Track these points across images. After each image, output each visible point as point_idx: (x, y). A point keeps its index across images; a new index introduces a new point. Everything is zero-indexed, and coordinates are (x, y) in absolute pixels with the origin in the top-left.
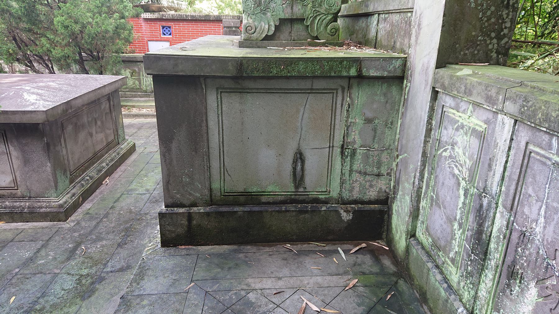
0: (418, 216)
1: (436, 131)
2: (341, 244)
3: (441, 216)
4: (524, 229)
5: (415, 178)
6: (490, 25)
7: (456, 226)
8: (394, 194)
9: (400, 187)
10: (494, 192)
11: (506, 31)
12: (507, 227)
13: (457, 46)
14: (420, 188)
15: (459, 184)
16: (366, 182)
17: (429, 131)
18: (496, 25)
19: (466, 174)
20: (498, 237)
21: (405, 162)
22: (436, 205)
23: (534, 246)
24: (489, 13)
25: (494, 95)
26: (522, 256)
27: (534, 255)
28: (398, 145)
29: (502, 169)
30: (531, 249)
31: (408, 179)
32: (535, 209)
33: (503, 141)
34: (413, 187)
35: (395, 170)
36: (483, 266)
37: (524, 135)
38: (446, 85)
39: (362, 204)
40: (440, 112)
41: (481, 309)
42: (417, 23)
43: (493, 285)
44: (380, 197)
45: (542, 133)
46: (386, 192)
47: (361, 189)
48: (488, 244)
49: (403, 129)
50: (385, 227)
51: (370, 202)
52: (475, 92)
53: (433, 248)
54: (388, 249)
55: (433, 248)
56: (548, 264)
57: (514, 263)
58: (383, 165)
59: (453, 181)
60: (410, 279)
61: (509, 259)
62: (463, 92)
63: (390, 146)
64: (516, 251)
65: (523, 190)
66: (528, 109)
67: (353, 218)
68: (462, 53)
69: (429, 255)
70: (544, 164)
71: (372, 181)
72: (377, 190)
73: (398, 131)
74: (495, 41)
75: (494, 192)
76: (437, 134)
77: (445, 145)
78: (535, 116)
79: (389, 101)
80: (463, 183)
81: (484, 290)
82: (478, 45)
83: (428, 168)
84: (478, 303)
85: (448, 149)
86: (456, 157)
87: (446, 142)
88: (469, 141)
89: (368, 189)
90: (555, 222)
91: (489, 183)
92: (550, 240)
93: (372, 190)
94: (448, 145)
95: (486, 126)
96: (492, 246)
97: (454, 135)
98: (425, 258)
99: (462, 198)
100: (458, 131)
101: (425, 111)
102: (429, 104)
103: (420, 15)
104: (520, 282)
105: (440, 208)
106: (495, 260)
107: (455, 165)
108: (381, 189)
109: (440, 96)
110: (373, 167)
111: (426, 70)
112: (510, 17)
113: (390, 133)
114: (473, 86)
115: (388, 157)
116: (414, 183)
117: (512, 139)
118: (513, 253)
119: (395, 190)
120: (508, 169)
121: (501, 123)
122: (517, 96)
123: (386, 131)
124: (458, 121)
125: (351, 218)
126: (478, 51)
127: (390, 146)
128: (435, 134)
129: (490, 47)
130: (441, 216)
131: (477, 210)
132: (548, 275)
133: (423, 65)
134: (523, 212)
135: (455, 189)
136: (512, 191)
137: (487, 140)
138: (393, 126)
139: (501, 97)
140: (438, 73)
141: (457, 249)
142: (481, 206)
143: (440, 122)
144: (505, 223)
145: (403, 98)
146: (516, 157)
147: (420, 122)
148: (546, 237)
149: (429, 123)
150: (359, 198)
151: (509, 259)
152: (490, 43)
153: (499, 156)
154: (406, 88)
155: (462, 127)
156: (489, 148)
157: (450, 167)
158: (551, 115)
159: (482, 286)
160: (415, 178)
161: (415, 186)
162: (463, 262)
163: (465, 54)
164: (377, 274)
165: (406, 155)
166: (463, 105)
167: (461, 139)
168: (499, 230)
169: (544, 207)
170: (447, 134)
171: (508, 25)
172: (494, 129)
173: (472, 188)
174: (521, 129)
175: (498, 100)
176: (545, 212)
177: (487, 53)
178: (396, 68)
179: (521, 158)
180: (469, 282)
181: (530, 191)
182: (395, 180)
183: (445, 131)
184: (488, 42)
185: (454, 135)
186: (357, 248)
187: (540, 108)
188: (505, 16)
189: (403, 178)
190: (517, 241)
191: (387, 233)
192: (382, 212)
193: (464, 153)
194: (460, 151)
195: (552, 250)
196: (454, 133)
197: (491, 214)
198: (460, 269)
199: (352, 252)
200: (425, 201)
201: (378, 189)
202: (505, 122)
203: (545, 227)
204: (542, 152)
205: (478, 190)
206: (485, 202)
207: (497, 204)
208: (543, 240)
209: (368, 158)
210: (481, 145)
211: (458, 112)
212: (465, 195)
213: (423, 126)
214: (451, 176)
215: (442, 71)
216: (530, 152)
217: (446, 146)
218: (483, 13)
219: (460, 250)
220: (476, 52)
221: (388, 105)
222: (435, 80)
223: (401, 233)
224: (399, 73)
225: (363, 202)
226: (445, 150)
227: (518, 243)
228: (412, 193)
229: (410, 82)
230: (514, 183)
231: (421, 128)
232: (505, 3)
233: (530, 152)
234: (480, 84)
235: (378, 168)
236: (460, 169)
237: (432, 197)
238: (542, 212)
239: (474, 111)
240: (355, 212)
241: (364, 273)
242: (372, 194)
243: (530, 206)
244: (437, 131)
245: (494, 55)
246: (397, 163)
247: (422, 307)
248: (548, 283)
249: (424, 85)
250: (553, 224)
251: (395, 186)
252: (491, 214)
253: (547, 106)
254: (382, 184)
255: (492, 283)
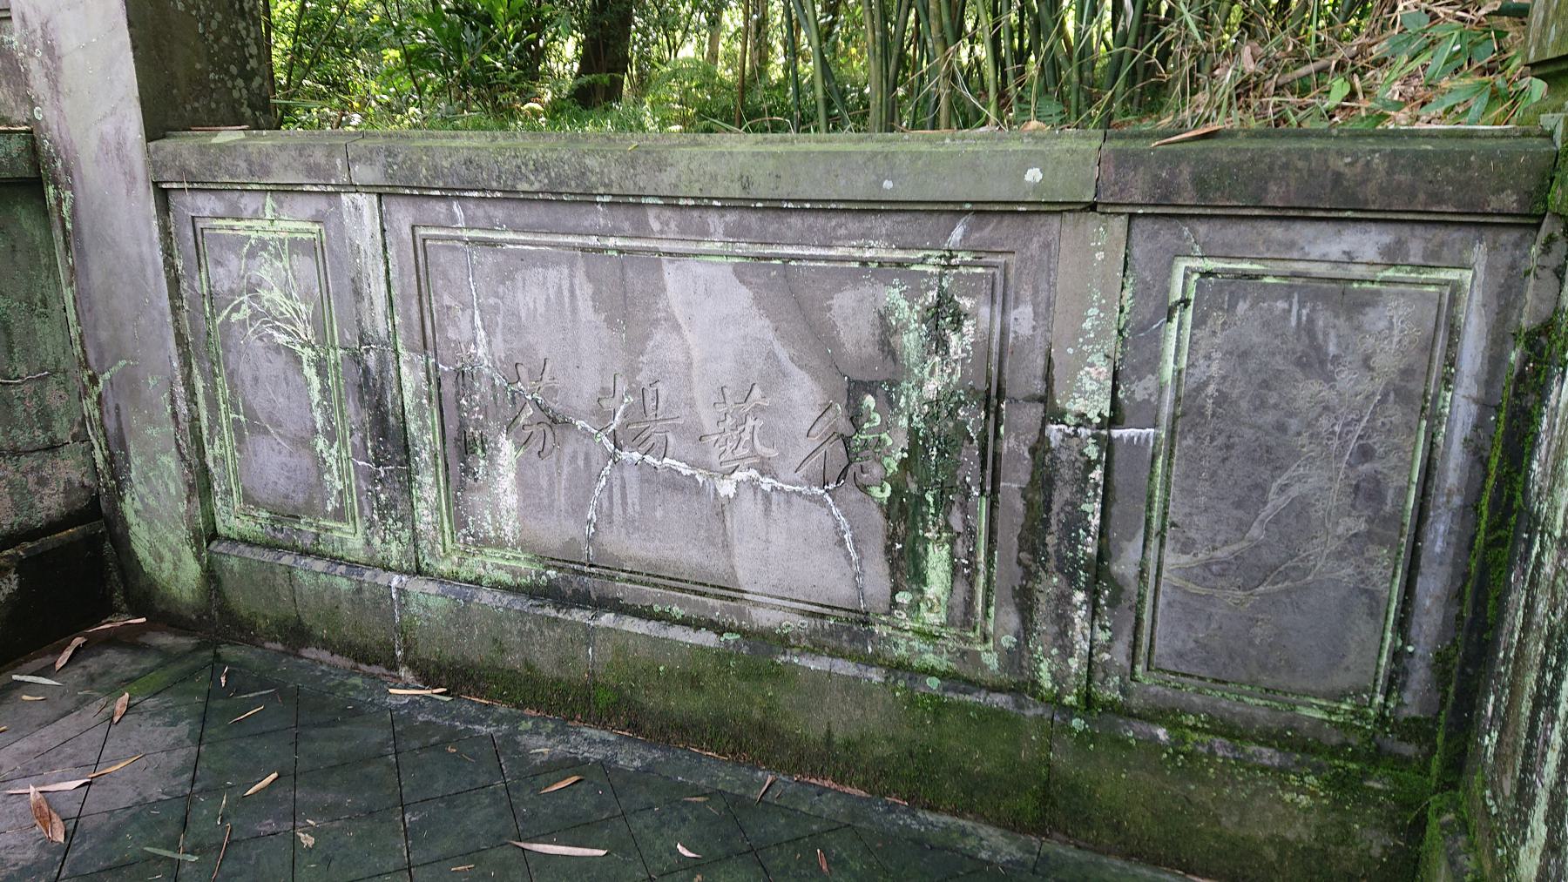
0: (209, 486)
1: (193, 278)
2: (15, 667)
3: (277, 448)
4: (459, 365)
5: (173, 401)
6: (222, 49)
7: (321, 443)
8: (113, 477)
9: (132, 447)
10: (383, 334)
11: (253, 63)
12: (429, 379)
13: (175, 91)
14: (195, 419)
15: (298, 360)
16: (25, 474)
17: (174, 282)
18: (233, 50)
19: (306, 331)
20: (420, 405)
21: (130, 383)
22: (251, 433)
23: (484, 380)
24: (214, 25)
25: (323, 161)
26: (472, 407)
27: (490, 392)
28: (84, 352)
29: (383, 287)
30: (482, 387)
31: (150, 415)
32: (464, 324)
33: (368, 239)
34: (177, 424)
35: (97, 416)
36: (409, 472)
37: (403, 216)
38: (193, 170)
39: (31, 540)
40: (191, 234)
41: (433, 548)
42: (39, 43)
43: (439, 491)
44: (73, 504)
45: (433, 203)
46: (83, 486)
47: (17, 497)
48: (405, 428)
49: (86, 307)
50: (115, 576)
51: (52, 527)
52: (275, 165)
53: (278, 526)
54: (144, 620)
55: (278, 526)
56: (513, 392)
57: (462, 427)
58: (56, 416)
59: (280, 362)
60: (242, 630)
61: (451, 428)
62: (246, 171)
63: (58, 362)
64: (459, 407)
65: (434, 306)
66: (401, 168)
67: (20, 584)
68: (188, 107)
69: (271, 546)
70: (454, 248)
71: (40, 467)
72: (61, 489)
73: (72, 317)
74: (240, 82)
75: (383, 334)
76: (197, 284)
77: (230, 297)
78: (415, 174)
79: (18, 247)
80: (307, 353)
81: (426, 512)
82: (213, 91)
83: (200, 368)
84: (422, 544)
85: (242, 302)
86: (268, 310)
87: (232, 291)
88: (291, 266)
89: (37, 492)
90: (500, 326)
91: (367, 323)
92: (503, 355)
93: (47, 491)
94: (240, 295)
95: (317, 227)
96: (413, 427)
97: (247, 269)
98: (268, 556)
99: (316, 383)
100: (254, 258)
101: (151, 239)
102: (155, 222)
103: (44, 25)
104: (484, 450)
105: (266, 432)
106: (428, 447)
107: (272, 328)
108: (69, 482)
109: (174, 200)
110: (32, 427)
111: (118, 150)
112: (253, 35)
113: (48, 330)
114: (267, 155)
115: (62, 392)
116: (175, 415)
117: (383, 230)
118: (455, 412)
119: (117, 466)
120: (394, 283)
121: (352, 210)
122: (371, 152)
123: (37, 326)
124: (249, 238)
125: (15, 585)
126: (217, 103)
127: (58, 362)
128: (192, 287)
129: (236, 94)
130: (277, 448)
131: (360, 386)
132: (519, 409)
133: (102, 139)
134: (448, 340)
135: (290, 374)
136: (416, 316)
137: (331, 250)
138: (49, 310)
139: (338, 161)
140: (157, 149)
141: (339, 485)
142: (366, 371)
143: (198, 254)
144: (422, 374)
145: (57, 233)
146: (401, 257)
147: (143, 270)
148: (496, 355)
149: (169, 265)
150: (20, 524)
151: (451, 428)
152: (234, 87)
153: (369, 267)
154: (59, 205)
155: (263, 245)
156: (340, 263)
157: (261, 339)
158: (442, 167)
159: (422, 509)
160: (173, 401)
161: (180, 420)
162: (363, 498)
163: (195, 110)
164: (160, 666)
165: (122, 363)
166: (248, 203)
167: (266, 270)
168: (417, 393)
169: (477, 312)
170: (223, 275)
171: (254, 50)
172: (341, 225)
173: (331, 350)
174: (393, 208)
175: (335, 167)
176: (482, 320)
177: (233, 107)
178: (12, 159)
179: (412, 255)
180: (391, 521)
181: (447, 300)
182: (107, 441)
183: (221, 270)
184: (229, 84)
185: (247, 269)
186: (68, 653)
187: (420, 160)
188: (244, 33)
189: (133, 420)
190: (454, 390)
191: (125, 587)
192: (93, 542)
193: (286, 296)
194: (277, 295)
195: (511, 369)
196: (246, 265)
197: (393, 373)
198: (361, 517)
199: (59, 666)
200: (217, 442)
201: (62, 485)
202: (360, 204)
203: (489, 343)
204: (443, 232)
205: (345, 349)
206: (371, 360)
207: (396, 351)
208: (494, 363)
209: (9, 406)
210: (321, 264)
211: (238, 219)
212: (321, 371)
213: (157, 275)
214: (272, 355)
215: (168, 145)
216: (424, 240)
217: (233, 300)
218: (204, 25)
219: (347, 482)
220: (213, 105)
221: (19, 255)
222: (154, 165)
223: (175, 552)
224: (24, 170)
225: (30, 534)
226: (237, 309)
227: (458, 393)
228: (177, 440)
229: (71, 187)
230: (415, 301)
231: (152, 282)
232: (237, 6)
233: (424, 240)
234: (282, 148)
235: (46, 428)
236: (289, 328)
237: (237, 422)
238: (478, 322)
239: (281, 206)
240: (22, 566)
241: (130, 680)
242: (51, 503)
243: (455, 325)
244: (197, 277)
245: (248, 112)
246: (100, 396)
247: (302, 657)
248: (522, 420)
249: (123, 185)
250: (499, 330)
251: (112, 454)
252: (393, 373)
253: (430, 153)
254: (69, 469)
255: (436, 490)
